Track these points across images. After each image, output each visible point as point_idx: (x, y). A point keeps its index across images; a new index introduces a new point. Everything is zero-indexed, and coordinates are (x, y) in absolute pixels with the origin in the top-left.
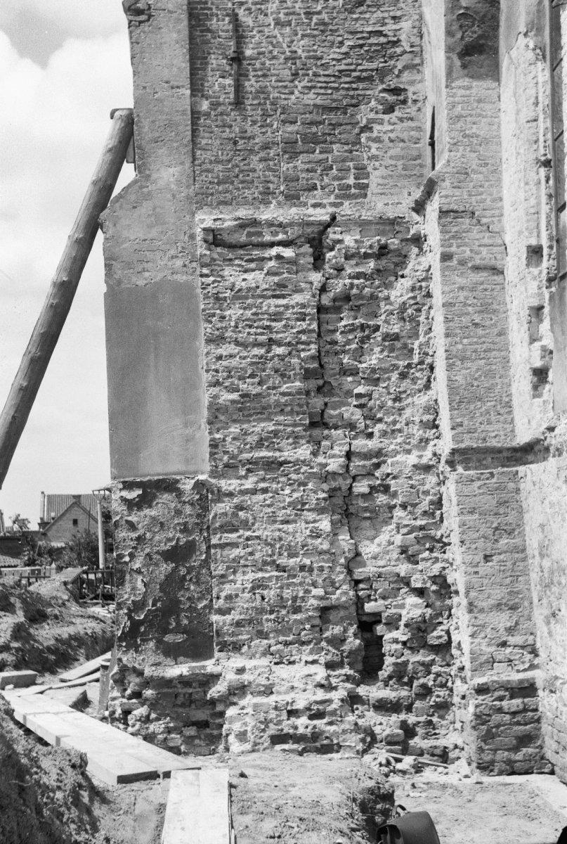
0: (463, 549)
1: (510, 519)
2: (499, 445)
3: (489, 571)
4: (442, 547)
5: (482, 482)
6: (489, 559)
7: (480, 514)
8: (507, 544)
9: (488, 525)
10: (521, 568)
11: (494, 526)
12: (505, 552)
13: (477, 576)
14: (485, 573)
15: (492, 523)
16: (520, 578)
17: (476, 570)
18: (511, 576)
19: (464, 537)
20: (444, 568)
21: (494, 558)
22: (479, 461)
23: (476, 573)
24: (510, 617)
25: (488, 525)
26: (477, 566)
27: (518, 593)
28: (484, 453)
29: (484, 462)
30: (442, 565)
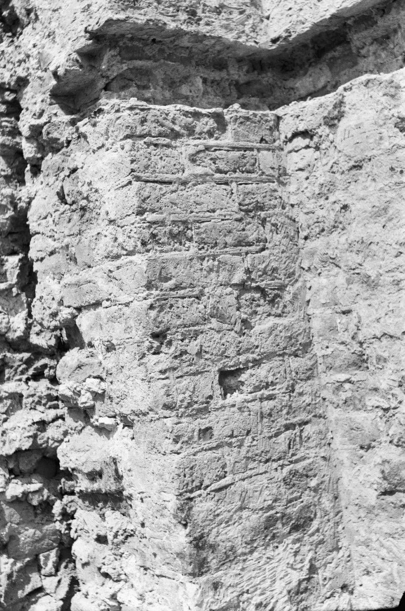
0: (164, 360)
1: (270, 257)
2: (230, 37)
3: (237, 421)
4: (29, 363)
5: (201, 143)
6: (232, 382)
7: (202, 243)
8: (272, 329)
9: (223, 276)
10: (307, 399)
11: (238, 277)
12: (269, 356)
13: (205, 444)
14: (228, 432)
15: (233, 268)
16: (309, 429)
17: (203, 423)
18: (288, 427)
19: (166, 317)
20: (42, 425)
21: (243, 377)
22: (172, 84)
23: (206, 432)
24: (296, 553)
25: (223, 276)
26: (204, 411)
27: (307, 475)
28: (185, 61)
29: (184, 90)
30: (37, 416)
